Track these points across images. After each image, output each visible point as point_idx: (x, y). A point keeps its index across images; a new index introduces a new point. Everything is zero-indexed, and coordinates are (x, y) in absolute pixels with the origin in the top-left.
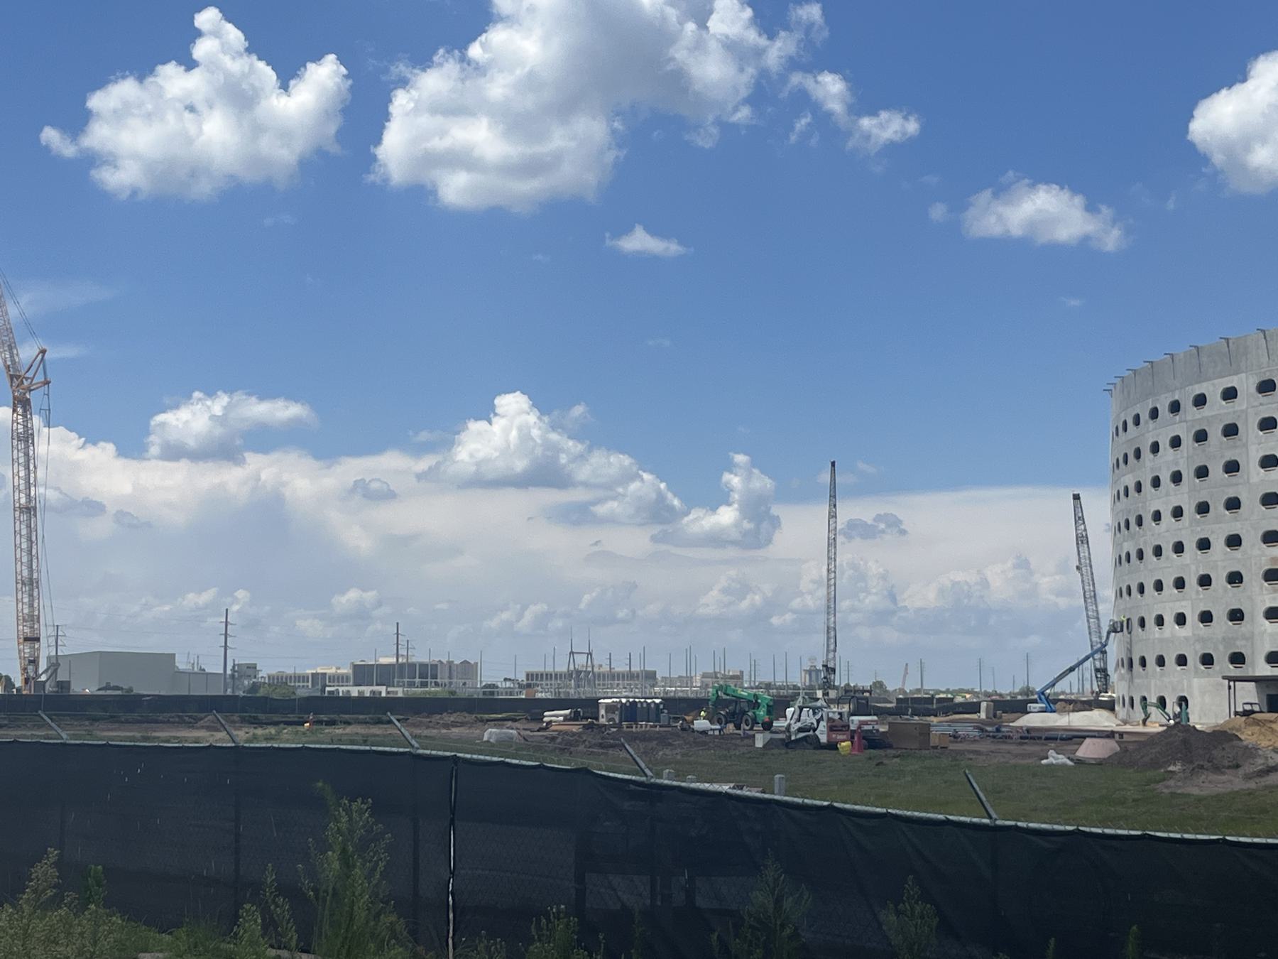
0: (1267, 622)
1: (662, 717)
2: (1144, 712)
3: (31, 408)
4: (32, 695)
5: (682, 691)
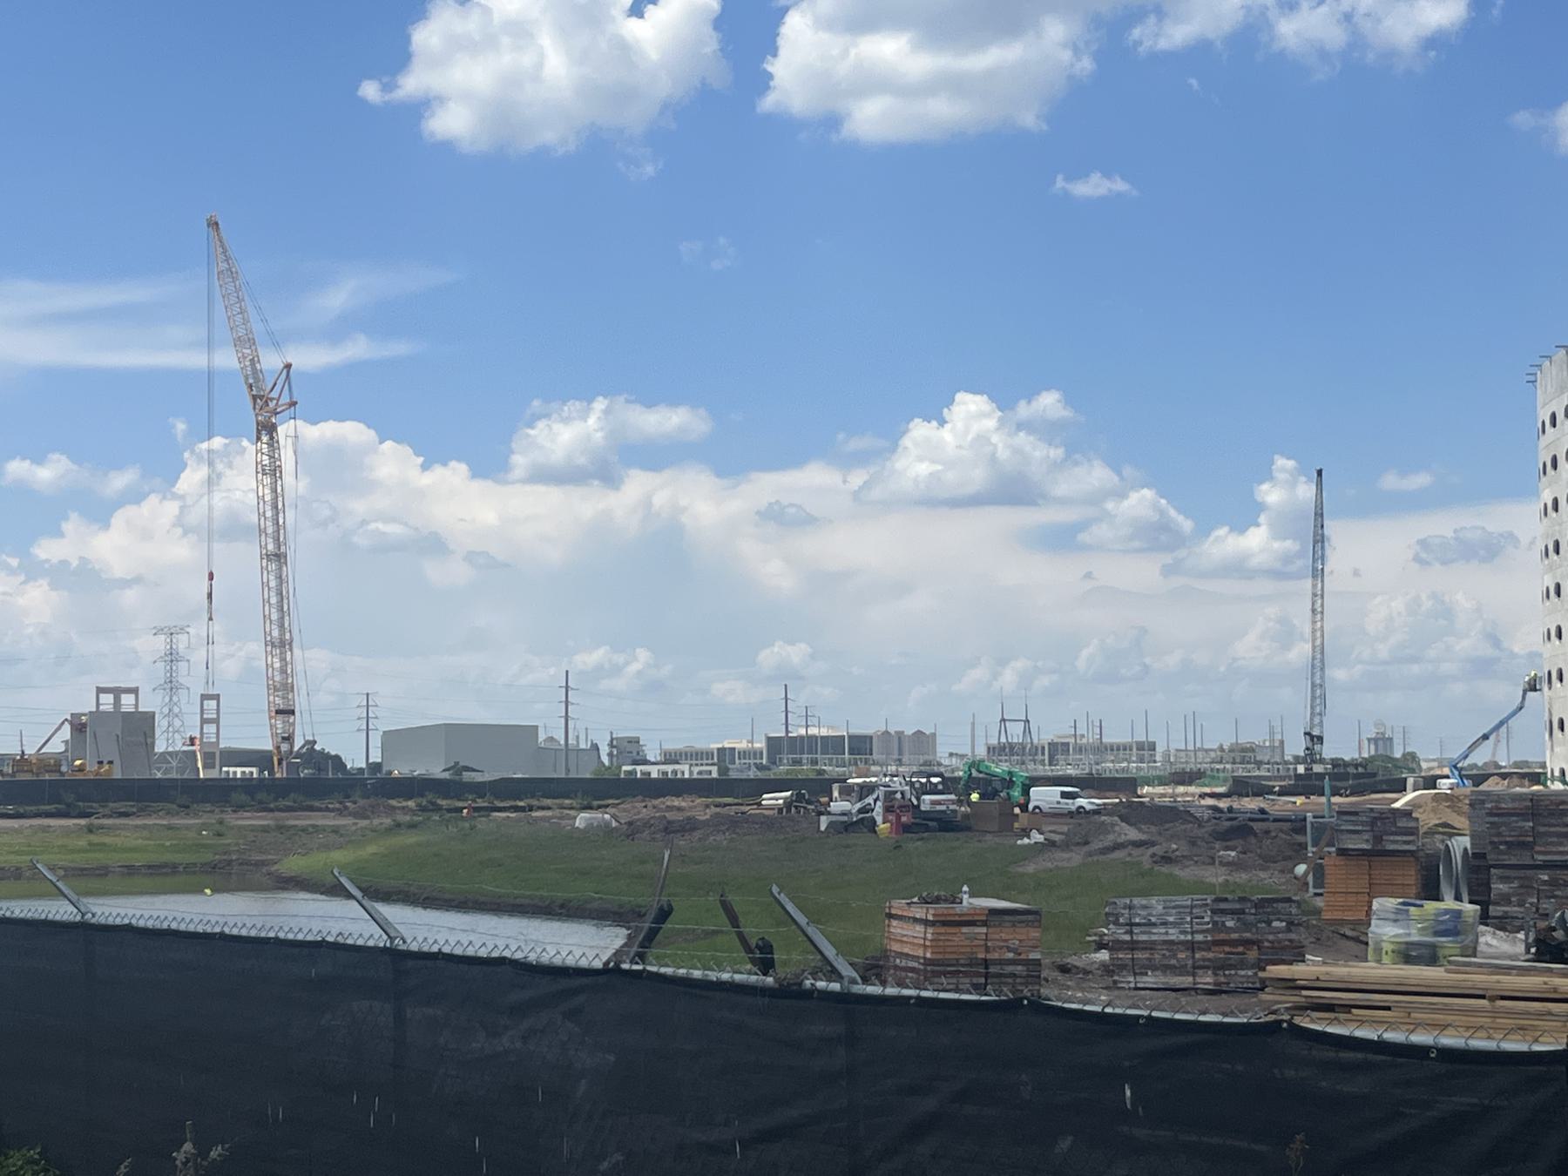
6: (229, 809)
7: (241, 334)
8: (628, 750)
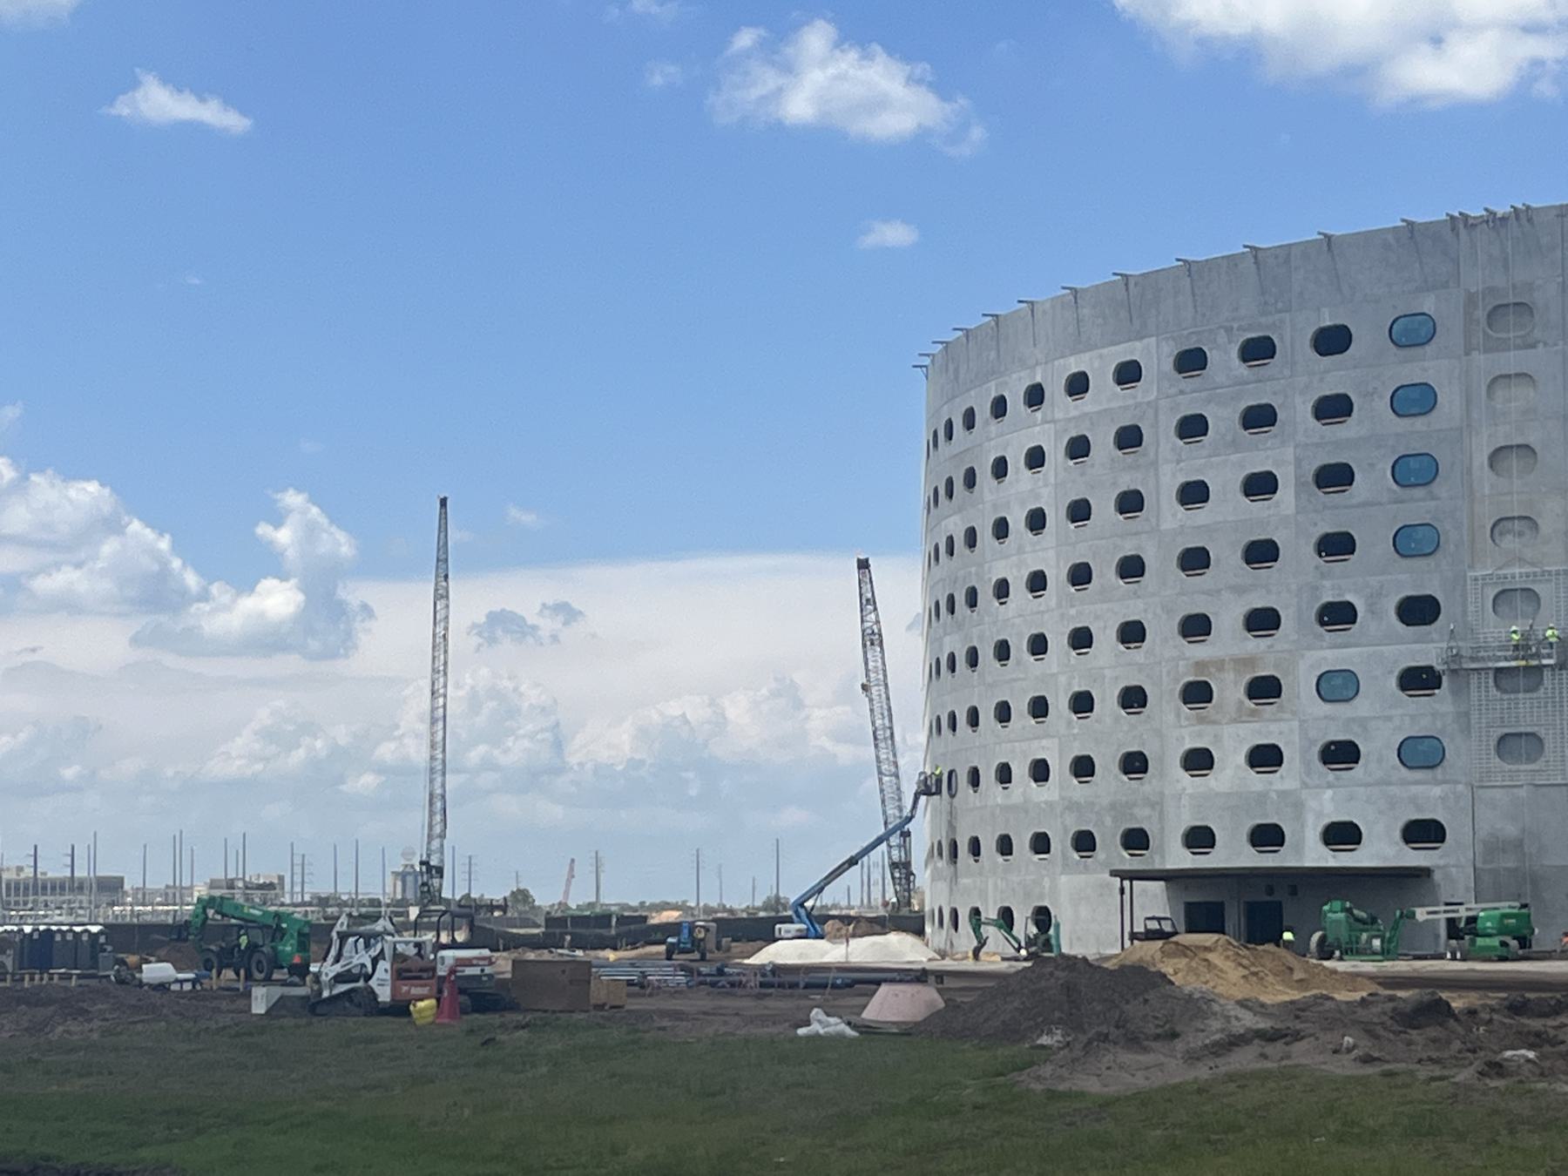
0: (1186, 775)
1: (100, 960)
2: (977, 937)
5: (167, 912)
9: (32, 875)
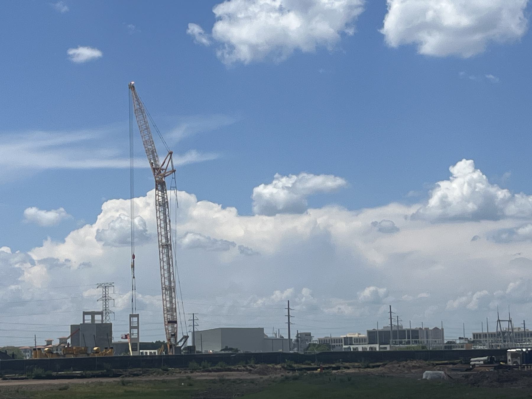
3: (166, 187)
4: (140, 356)
6: (189, 371)
7: (146, 139)
8: (306, 339)
9: (523, 330)
